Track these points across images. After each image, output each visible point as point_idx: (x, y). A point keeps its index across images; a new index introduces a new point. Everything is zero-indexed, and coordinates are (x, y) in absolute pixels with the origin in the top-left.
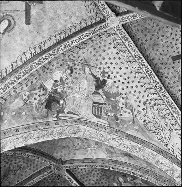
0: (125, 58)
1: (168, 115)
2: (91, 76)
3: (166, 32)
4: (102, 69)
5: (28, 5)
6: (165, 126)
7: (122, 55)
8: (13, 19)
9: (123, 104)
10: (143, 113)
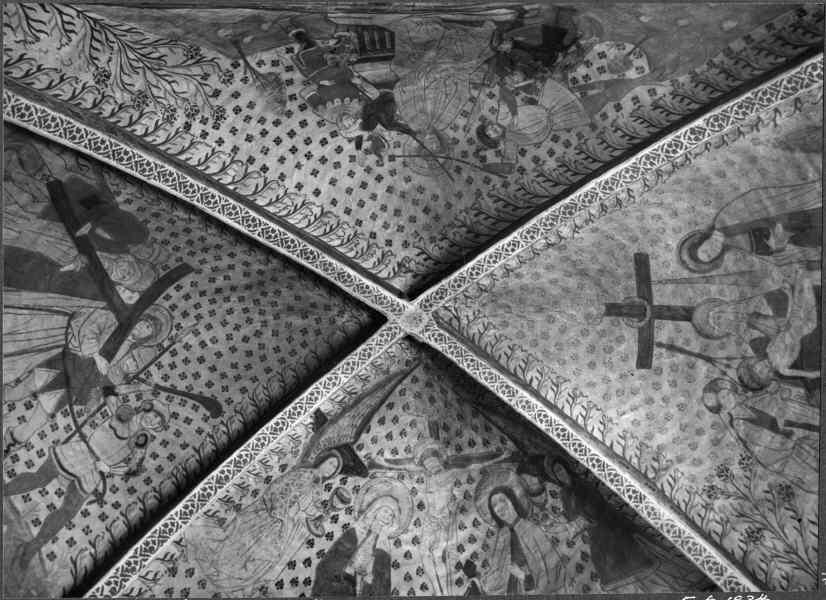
0: (333, 222)
1: (134, 119)
2: (413, 127)
3: (242, 322)
4: (386, 159)
5: (644, 298)
6: (126, 79)
7: (345, 226)
8: (683, 263)
9: (290, 82)
10: (214, 82)
